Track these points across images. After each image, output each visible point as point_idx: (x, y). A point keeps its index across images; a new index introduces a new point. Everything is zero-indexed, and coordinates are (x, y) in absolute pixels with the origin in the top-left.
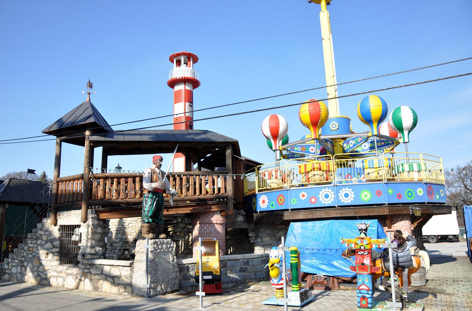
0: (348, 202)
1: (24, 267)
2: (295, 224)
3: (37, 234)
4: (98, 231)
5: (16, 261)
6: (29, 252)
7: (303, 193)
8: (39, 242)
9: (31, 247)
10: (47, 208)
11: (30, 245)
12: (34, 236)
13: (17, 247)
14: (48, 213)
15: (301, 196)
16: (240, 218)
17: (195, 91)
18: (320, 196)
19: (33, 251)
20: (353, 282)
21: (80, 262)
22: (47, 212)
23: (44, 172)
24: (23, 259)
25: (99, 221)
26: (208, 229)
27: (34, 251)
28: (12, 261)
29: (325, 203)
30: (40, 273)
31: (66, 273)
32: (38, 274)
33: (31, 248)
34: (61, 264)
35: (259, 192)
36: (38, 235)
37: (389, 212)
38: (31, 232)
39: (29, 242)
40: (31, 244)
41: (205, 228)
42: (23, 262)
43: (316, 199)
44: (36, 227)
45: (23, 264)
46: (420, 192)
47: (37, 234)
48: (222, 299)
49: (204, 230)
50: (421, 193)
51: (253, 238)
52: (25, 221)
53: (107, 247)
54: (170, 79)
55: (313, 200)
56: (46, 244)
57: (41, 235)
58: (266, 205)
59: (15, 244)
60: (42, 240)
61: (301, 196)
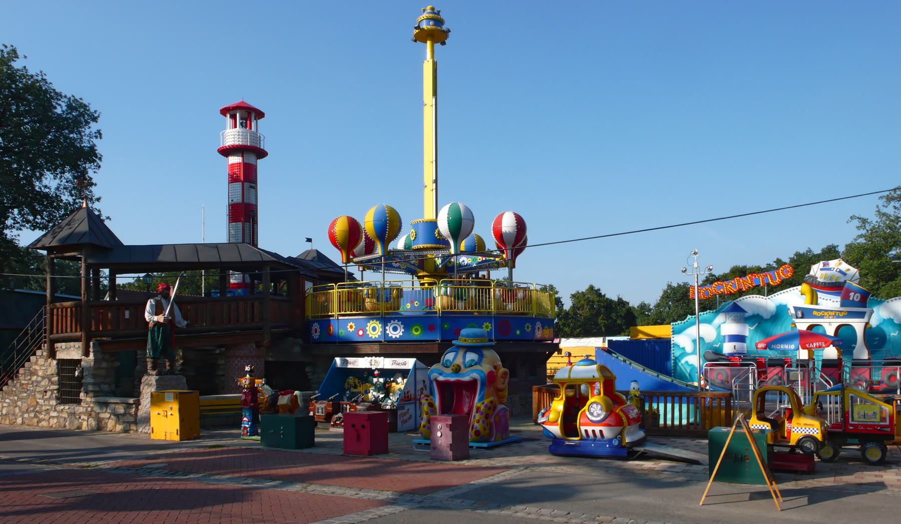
0: (396, 337)
1: (17, 408)
2: (358, 360)
3: (31, 369)
4: (102, 366)
5: (7, 401)
6: (23, 390)
7: (351, 324)
8: (34, 378)
9: (24, 384)
10: (42, 339)
11: (23, 382)
12: (27, 371)
13: (23, 366)
14: (43, 345)
15: (348, 327)
16: (297, 349)
17: (261, 164)
18: (367, 328)
19: (27, 389)
20: (790, 448)
21: (83, 401)
22: (42, 343)
23: (96, 185)
24: (16, 398)
25: (103, 355)
26: (239, 363)
27: (28, 388)
28: (2, 401)
29: (372, 337)
30: (37, 414)
31: (67, 413)
32: (35, 414)
33: (24, 386)
34: (303, 396)
35: (420, 285)
36: (33, 371)
37: (439, 351)
38: (23, 366)
39: (21, 378)
40: (25, 380)
41: (236, 362)
42: (16, 402)
43: (363, 332)
44: (29, 360)
45: (16, 404)
46: (541, 316)
47: (31, 369)
48: (628, 498)
49: (236, 364)
50: (487, 326)
51: (310, 374)
52: (14, 353)
53: (135, 383)
54: (221, 146)
55: (361, 333)
56: (42, 380)
57: (36, 370)
58: (369, 326)
59: (27, 356)
60: (38, 376)
61: (348, 327)
